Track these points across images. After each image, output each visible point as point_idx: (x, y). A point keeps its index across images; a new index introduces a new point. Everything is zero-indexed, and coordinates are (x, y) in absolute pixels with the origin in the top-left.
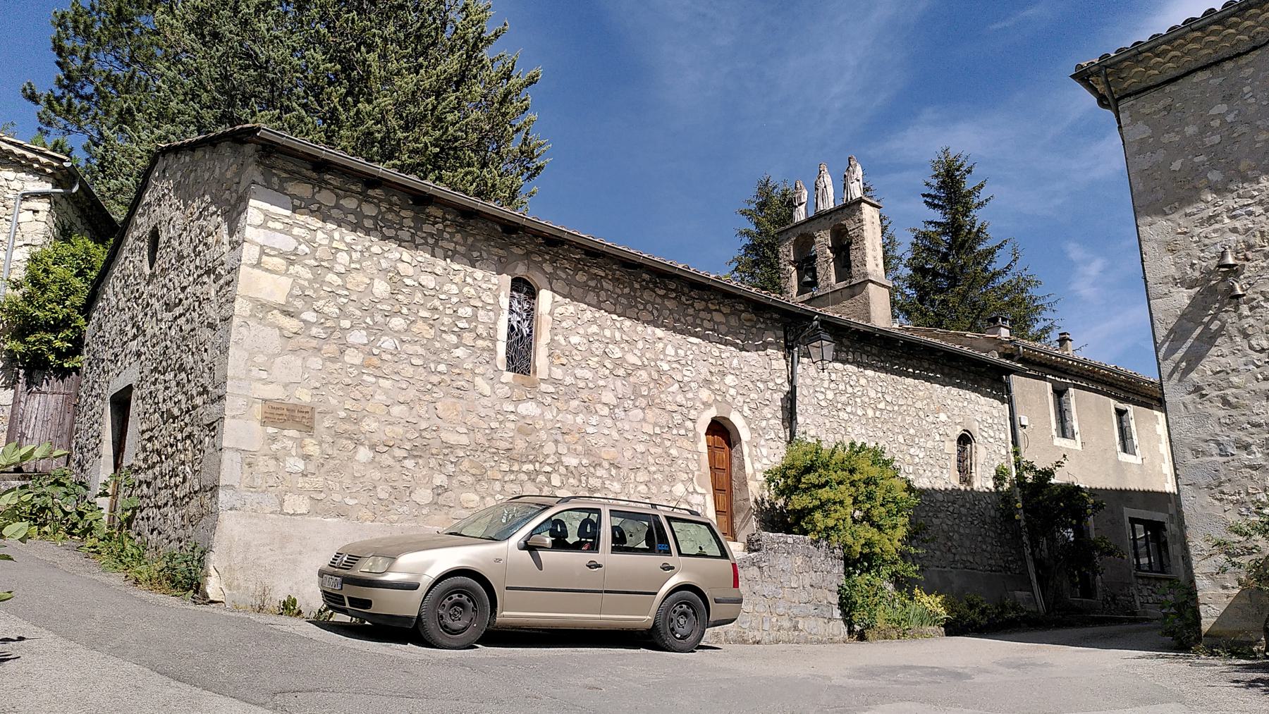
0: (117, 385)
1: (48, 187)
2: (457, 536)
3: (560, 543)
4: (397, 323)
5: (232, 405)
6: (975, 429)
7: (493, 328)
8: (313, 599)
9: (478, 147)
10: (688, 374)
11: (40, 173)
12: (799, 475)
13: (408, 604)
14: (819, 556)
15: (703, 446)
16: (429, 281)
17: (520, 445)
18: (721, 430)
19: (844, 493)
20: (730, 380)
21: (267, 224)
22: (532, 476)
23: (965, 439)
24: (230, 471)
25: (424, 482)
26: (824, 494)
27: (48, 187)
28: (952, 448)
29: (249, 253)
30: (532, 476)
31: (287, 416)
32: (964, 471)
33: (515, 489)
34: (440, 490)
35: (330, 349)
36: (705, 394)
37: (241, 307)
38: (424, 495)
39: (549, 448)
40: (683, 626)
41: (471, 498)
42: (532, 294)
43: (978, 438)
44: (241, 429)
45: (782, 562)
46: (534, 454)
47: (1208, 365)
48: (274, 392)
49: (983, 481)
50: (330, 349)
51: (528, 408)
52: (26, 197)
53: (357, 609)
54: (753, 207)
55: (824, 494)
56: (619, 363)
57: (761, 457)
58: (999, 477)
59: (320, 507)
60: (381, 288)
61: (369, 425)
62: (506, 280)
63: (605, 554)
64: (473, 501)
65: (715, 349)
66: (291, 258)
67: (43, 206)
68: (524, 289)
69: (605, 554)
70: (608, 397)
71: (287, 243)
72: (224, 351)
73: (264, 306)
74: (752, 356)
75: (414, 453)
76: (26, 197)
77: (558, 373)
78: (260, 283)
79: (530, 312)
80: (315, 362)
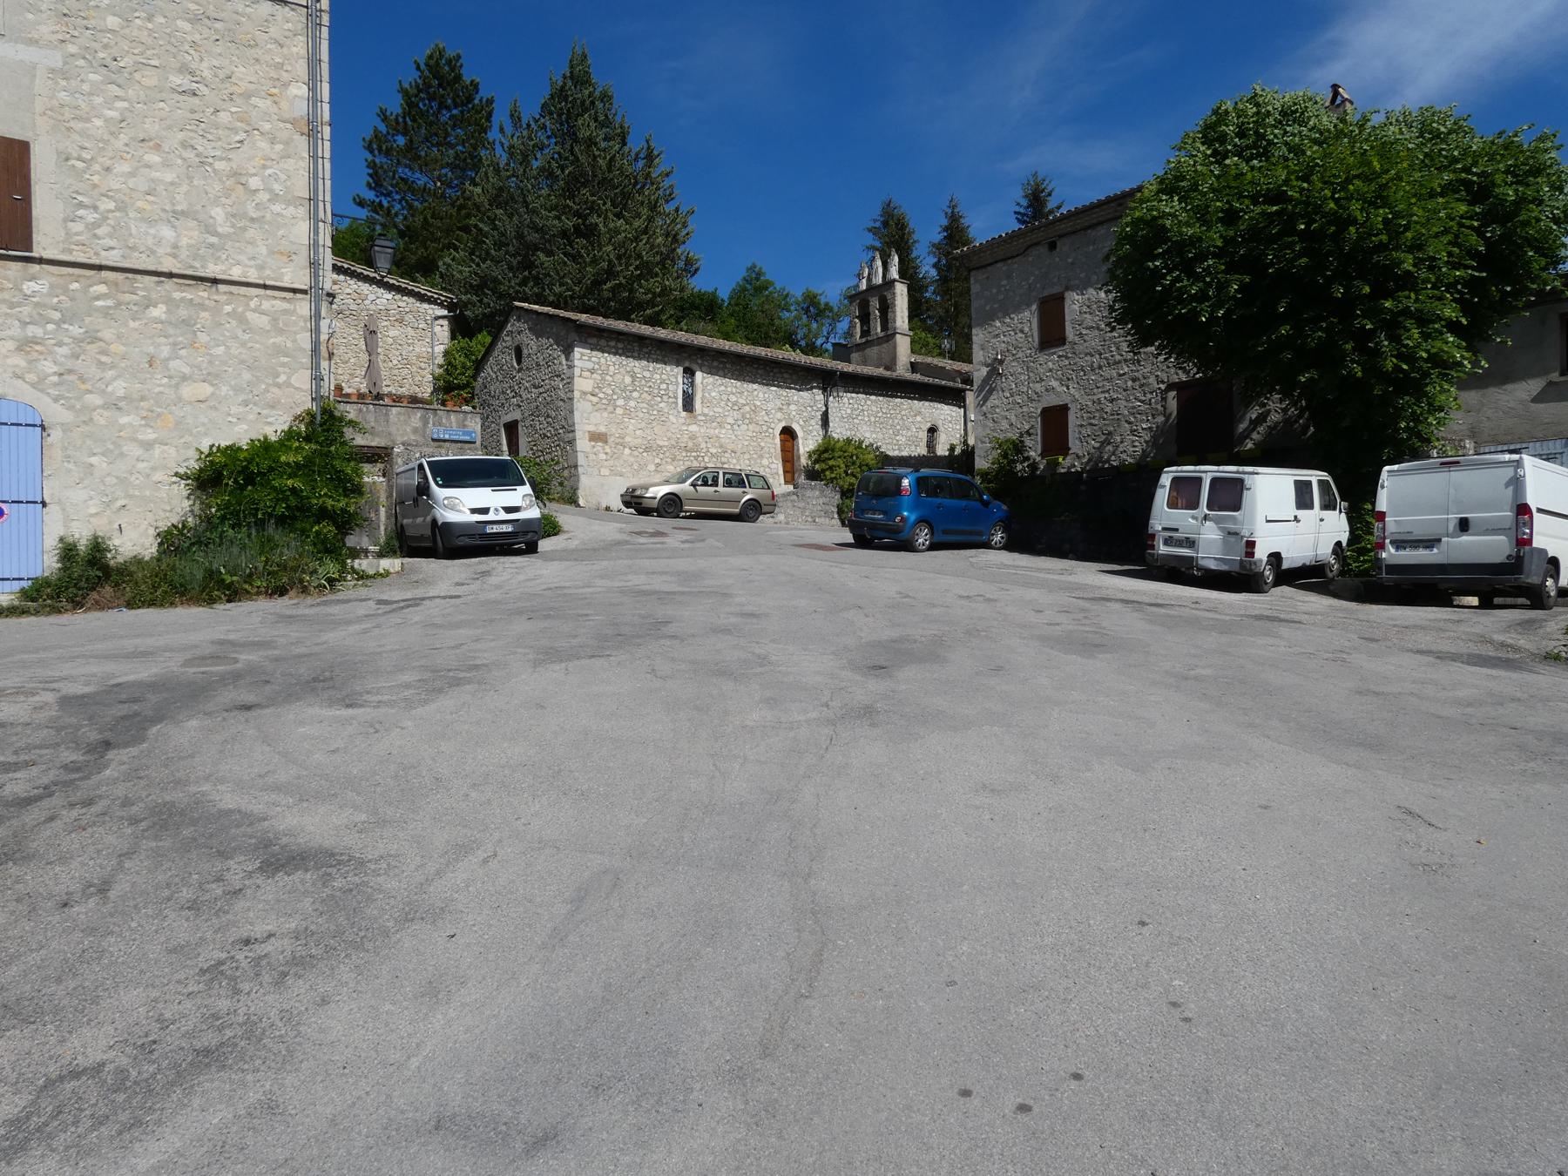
0: (509, 418)
1: (445, 312)
2: (667, 482)
3: (705, 484)
4: (635, 394)
5: (578, 434)
6: (940, 424)
7: (675, 392)
8: (617, 504)
9: (662, 263)
10: (770, 406)
11: (441, 305)
12: (826, 451)
13: (655, 504)
14: (828, 491)
15: (778, 441)
16: (647, 374)
17: (690, 444)
18: (788, 434)
19: (840, 462)
20: (793, 407)
21: (583, 357)
22: (696, 458)
23: (932, 430)
24: (581, 460)
25: (651, 461)
26: (831, 463)
27: (445, 312)
28: (924, 435)
29: (577, 371)
30: (696, 458)
31: (597, 437)
32: (931, 445)
33: (688, 464)
34: (658, 465)
35: (610, 408)
36: (779, 415)
37: (577, 394)
38: (652, 467)
39: (703, 445)
40: (751, 514)
41: (671, 468)
42: (693, 374)
43: (941, 428)
44: (583, 444)
45: (809, 493)
46: (696, 448)
47: (989, 404)
48: (592, 428)
49: (942, 450)
50: (610, 408)
51: (693, 428)
52: (437, 318)
53: (635, 502)
54: (878, 224)
55: (831, 463)
56: (735, 404)
57: (807, 444)
58: (952, 449)
59: (613, 473)
60: (628, 380)
61: (628, 439)
62: (681, 369)
63: (720, 488)
64: (672, 469)
65: (784, 392)
66: (592, 371)
67: (445, 323)
68: (690, 373)
69: (720, 488)
70: (730, 420)
71: (590, 365)
72: (572, 412)
73: (585, 393)
74: (805, 394)
75: (647, 450)
76: (437, 318)
77: (706, 411)
78: (582, 384)
79: (692, 384)
80: (605, 414)
